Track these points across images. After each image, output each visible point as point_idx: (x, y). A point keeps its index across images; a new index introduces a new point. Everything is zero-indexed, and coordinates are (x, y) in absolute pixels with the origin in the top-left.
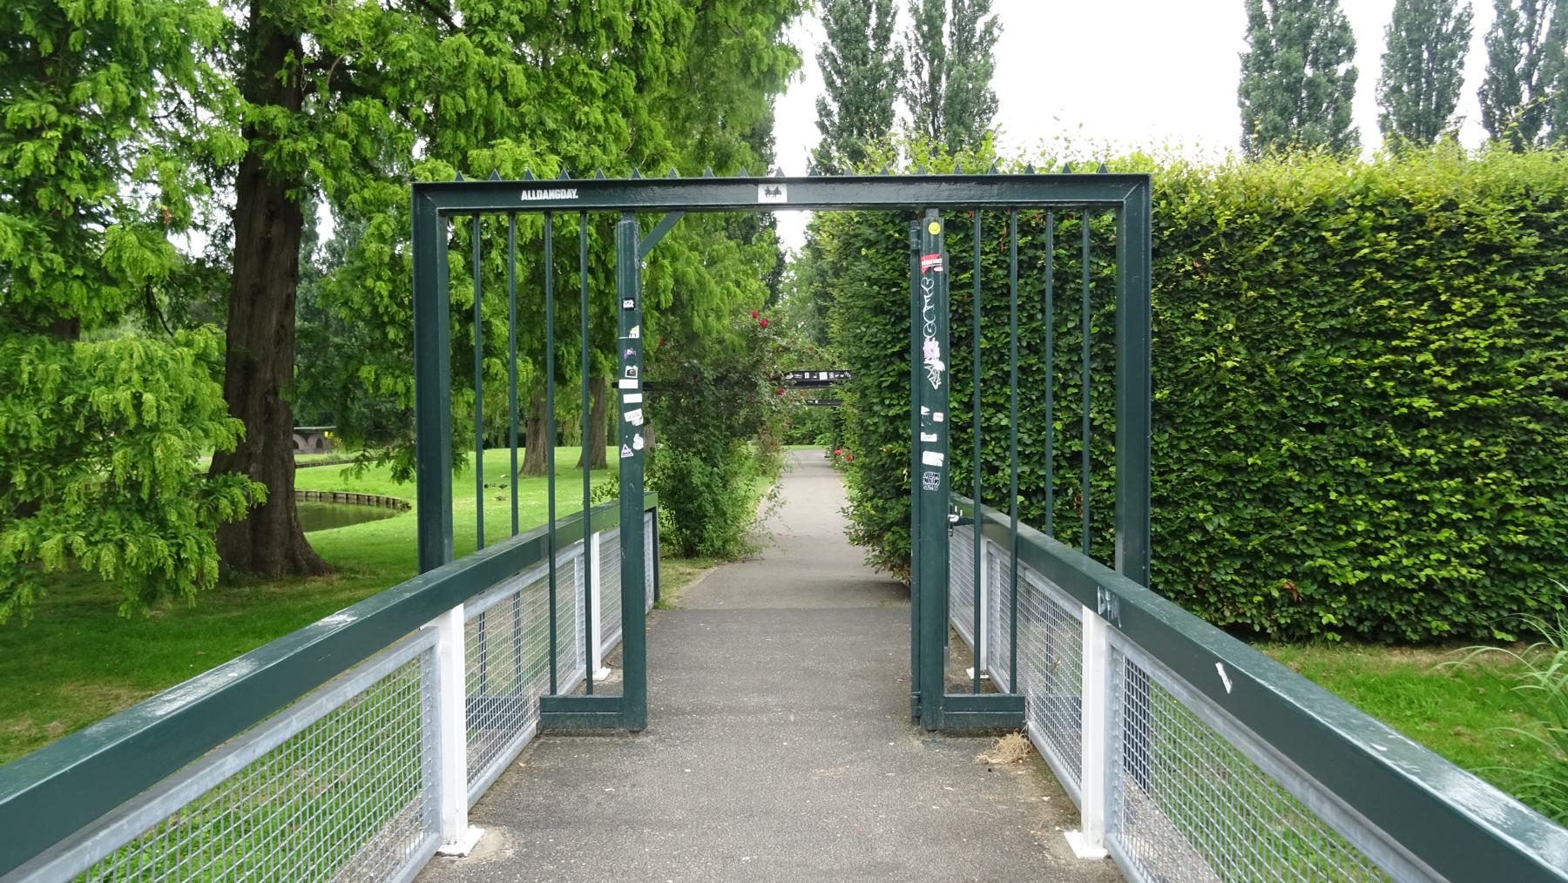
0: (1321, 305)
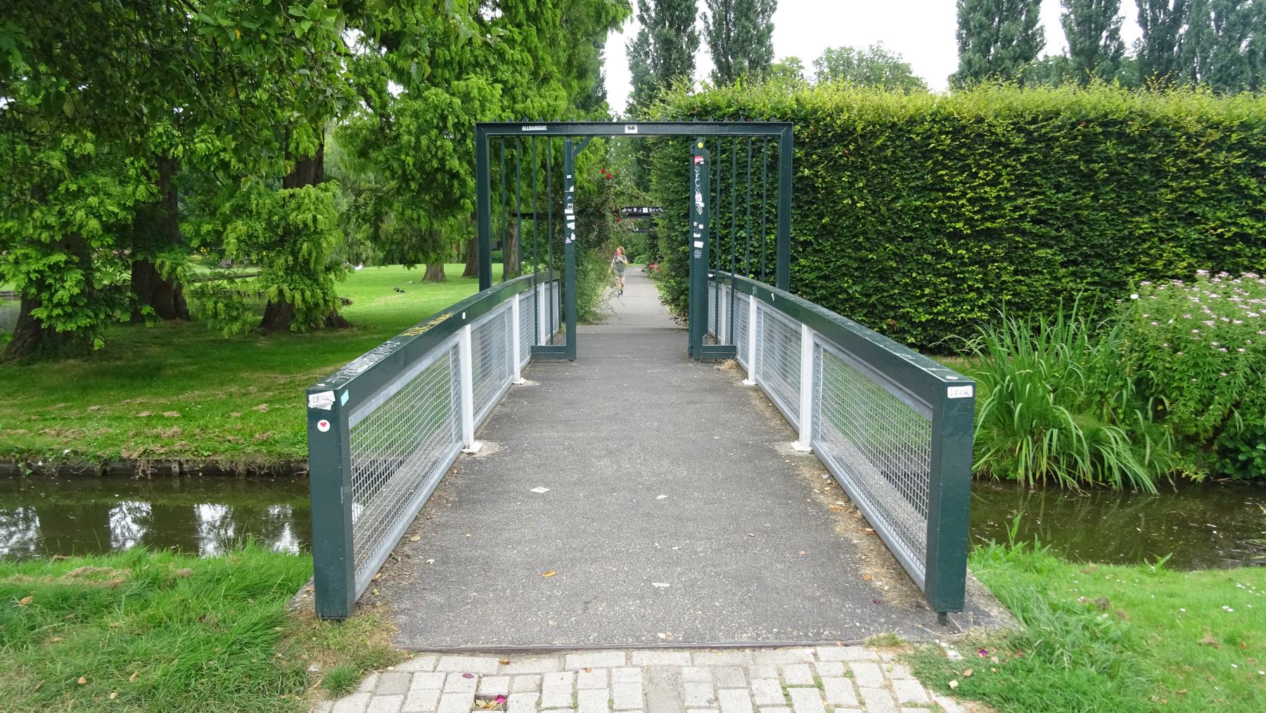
0: (912, 173)
